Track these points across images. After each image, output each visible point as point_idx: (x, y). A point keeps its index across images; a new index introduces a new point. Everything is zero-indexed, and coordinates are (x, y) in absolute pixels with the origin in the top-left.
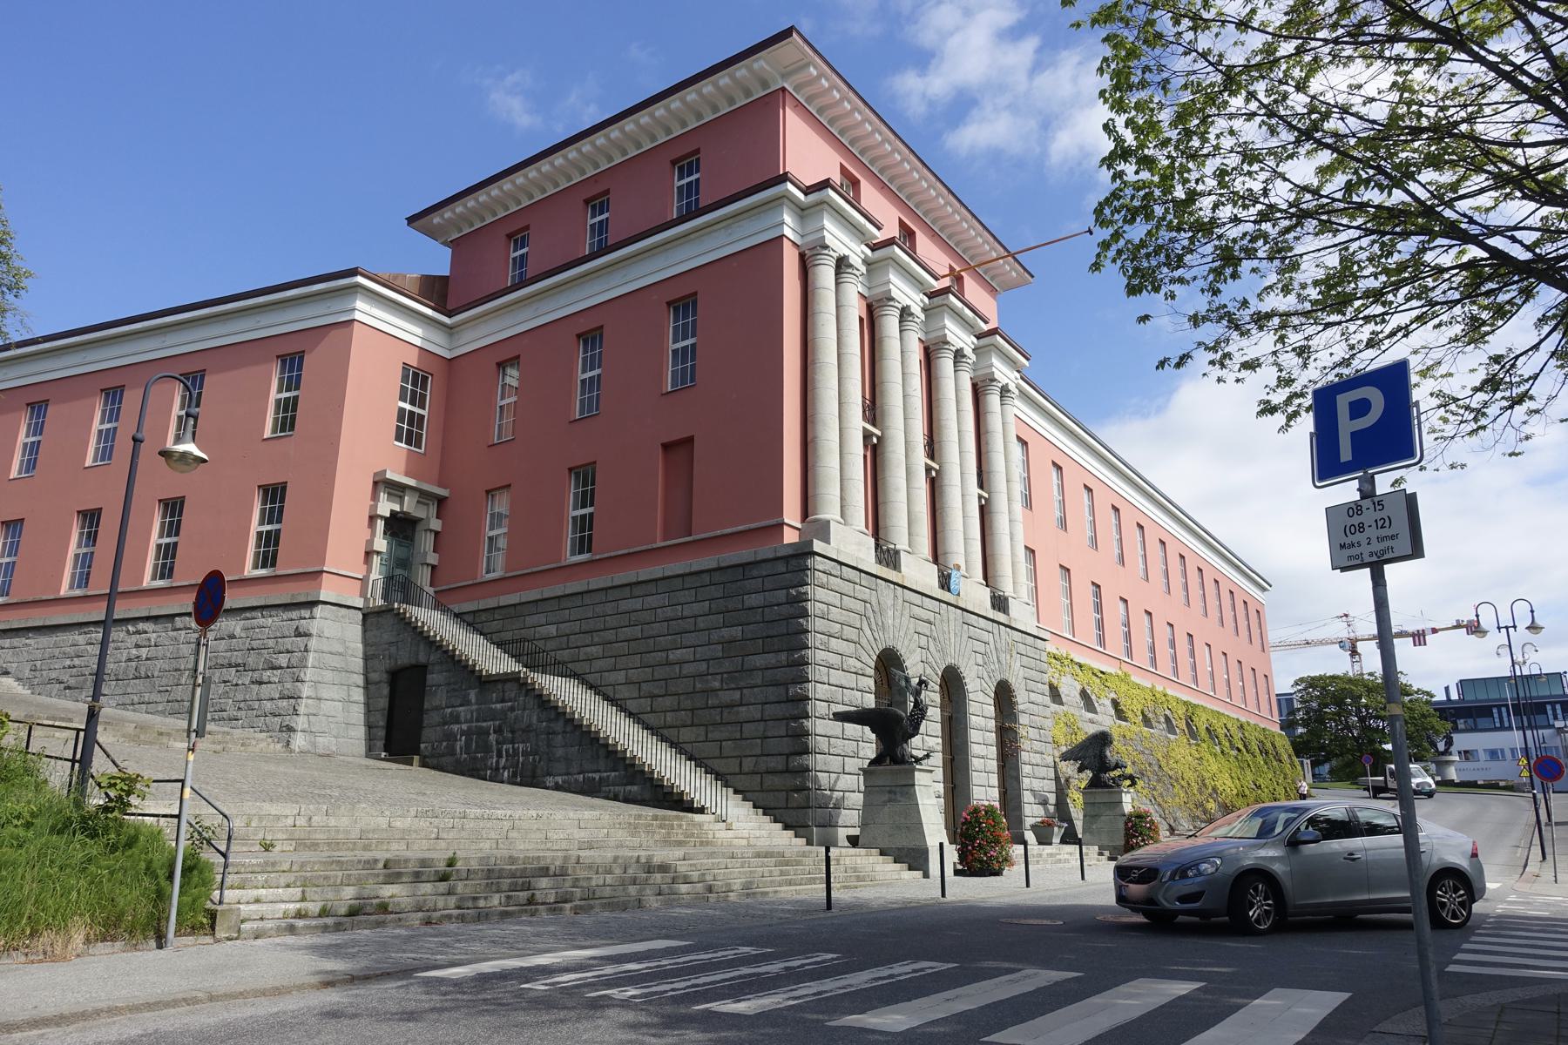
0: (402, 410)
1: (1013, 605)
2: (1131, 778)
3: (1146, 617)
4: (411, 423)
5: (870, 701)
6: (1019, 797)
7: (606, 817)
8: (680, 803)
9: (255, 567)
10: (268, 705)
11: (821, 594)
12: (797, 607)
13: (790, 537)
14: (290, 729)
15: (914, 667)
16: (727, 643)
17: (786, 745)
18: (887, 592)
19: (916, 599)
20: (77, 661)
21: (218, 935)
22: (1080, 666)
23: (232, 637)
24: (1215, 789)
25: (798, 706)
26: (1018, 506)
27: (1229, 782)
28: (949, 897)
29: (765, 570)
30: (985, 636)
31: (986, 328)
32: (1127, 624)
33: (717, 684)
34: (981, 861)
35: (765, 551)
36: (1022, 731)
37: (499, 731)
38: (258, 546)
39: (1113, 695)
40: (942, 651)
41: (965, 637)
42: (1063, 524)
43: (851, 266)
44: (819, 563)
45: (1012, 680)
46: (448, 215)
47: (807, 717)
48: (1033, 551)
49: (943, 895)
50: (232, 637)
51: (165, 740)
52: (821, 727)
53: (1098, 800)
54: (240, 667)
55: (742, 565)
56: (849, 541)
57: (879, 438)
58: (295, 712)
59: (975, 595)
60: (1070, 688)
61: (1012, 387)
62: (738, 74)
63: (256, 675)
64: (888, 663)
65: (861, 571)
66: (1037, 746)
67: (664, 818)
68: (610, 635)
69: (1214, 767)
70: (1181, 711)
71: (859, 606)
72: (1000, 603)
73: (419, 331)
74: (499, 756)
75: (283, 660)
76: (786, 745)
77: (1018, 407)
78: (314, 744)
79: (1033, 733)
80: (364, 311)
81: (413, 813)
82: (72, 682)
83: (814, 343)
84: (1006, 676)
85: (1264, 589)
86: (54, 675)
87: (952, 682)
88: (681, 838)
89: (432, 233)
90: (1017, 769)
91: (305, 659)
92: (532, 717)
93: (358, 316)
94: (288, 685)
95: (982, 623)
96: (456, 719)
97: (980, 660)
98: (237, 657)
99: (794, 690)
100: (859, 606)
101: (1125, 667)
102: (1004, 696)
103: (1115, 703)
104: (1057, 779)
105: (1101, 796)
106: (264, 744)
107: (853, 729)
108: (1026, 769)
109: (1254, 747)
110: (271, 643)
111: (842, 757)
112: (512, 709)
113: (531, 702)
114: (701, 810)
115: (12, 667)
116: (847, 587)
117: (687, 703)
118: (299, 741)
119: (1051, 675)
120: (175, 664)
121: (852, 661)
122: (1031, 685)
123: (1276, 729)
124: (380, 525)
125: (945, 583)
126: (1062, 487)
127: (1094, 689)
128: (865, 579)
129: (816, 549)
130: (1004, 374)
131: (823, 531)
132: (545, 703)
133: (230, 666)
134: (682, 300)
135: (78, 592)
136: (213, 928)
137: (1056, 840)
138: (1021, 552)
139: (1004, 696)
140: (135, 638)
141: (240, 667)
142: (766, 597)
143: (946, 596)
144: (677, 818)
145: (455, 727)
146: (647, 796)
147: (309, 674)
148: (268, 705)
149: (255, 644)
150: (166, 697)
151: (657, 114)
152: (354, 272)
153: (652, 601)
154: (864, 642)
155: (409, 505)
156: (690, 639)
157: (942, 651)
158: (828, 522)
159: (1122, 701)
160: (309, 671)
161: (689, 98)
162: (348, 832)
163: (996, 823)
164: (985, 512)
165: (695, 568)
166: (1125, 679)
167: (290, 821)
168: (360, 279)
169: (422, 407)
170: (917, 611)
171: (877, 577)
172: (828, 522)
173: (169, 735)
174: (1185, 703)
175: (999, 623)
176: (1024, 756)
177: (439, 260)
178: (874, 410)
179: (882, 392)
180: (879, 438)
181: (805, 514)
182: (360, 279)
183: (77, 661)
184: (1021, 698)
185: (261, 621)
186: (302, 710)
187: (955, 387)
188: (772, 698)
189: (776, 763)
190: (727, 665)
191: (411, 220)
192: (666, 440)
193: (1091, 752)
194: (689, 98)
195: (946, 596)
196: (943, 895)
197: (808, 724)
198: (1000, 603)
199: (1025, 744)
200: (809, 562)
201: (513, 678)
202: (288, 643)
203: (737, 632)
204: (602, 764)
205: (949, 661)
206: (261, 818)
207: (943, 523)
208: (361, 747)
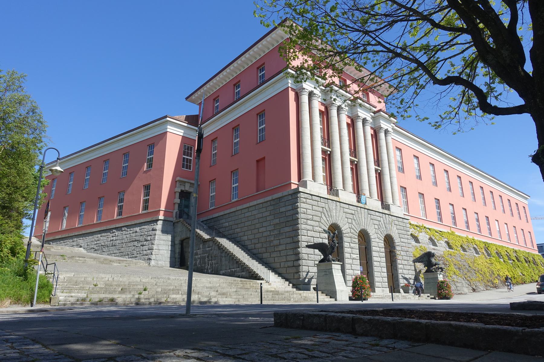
0: (184, 158)
1: (392, 208)
2: (441, 268)
3: (464, 211)
4: (187, 162)
5: (326, 241)
6: (397, 276)
7: (222, 281)
8: (254, 276)
10: (145, 252)
11: (303, 205)
12: (295, 210)
13: (293, 187)
14: (150, 259)
15: (345, 228)
17: (293, 258)
18: (332, 205)
19: (347, 206)
20: (98, 242)
22: (429, 229)
23: (136, 232)
24: (498, 275)
26: (394, 172)
28: (320, 303)
30: (379, 219)
32: (454, 213)
33: (272, 239)
34: (358, 295)
36: (398, 253)
37: (208, 257)
39: (446, 240)
41: (369, 219)
43: (315, 94)
44: (302, 195)
45: (393, 235)
47: (299, 248)
51: (111, 263)
52: (304, 251)
54: (138, 241)
55: (279, 198)
56: (316, 187)
57: (330, 152)
58: (152, 254)
60: (423, 237)
61: (390, 129)
63: (142, 243)
64: (335, 231)
65: (321, 197)
67: (245, 281)
69: (499, 267)
71: (321, 209)
72: (385, 206)
73: (183, 131)
75: (149, 238)
76: (293, 258)
77: (393, 135)
78: (158, 264)
79: (402, 253)
81: (150, 278)
82: (97, 248)
83: (301, 122)
84: (389, 233)
85: (526, 199)
86: (92, 246)
87: (364, 237)
89: (193, 102)
90: (396, 266)
91: (155, 237)
92: (216, 252)
93: (168, 130)
96: (196, 254)
97: (376, 227)
98: (137, 238)
99: (295, 240)
100: (321, 209)
101: (453, 230)
102: (389, 241)
103: (448, 243)
104: (415, 270)
105: (430, 275)
106: (142, 263)
107: (311, 251)
108: (400, 266)
109: (522, 259)
110: (146, 233)
111: (310, 261)
112: (211, 250)
113: (216, 248)
114: (262, 279)
115: (82, 245)
117: (265, 245)
118: (153, 263)
122: (401, 236)
123: (537, 253)
124: (177, 195)
125: (359, 201)
128: (322, 200)
129: (300, 190)
130: (384, 125)
131: (305, 185)
132: (221, 248)
133: (135, 241)
134: (260, 113)
135: (99, 222)
137: (411, 291)
138: (397, 189)
139: (389, 241)
141: (138, 241)
142: (285, 207)
143: (360, 205)
144: (245, 281)
145: (197, 257)
146: (247, 275)
147: (156, 242)
149: (142, 234)
150: (119, 251)
151: (255, 50)
152: (166, 117)
154: (322, 221)
155: (187, 188)
157: (359, 224)
158: (306, 181)
159: (451, 242)
160: (156, 241)
161: (264, 43)
162: (124, 282)
163: (363, 282)
164: (380, 176)
165: (266, 200)
166: (453, 234)
167: (107, 279)
169: (191, 156)
170: (346, 210)
171: (328, 199)
173: (113, 261)
174: (484, 243)
176: (399, 262)
177: (194, 110)
178: (354, 152)
180: (330, 152)
181: (300, 178)
182: (168, 119)
183: (98, 242)
184: (397, 240)
185: (144, 227)
186: (153, 253)
189: (290, 264)
191: (187, 98)
194: (264, 43)
195: (360, 205)
197: (299, 250)
198: (385, 206)
199: (399, 257)
202: (151, 233)
203: (277, 221)
204: (235, 266)
205: (362, 227)
207: (361, 180)
208: (168, 264)
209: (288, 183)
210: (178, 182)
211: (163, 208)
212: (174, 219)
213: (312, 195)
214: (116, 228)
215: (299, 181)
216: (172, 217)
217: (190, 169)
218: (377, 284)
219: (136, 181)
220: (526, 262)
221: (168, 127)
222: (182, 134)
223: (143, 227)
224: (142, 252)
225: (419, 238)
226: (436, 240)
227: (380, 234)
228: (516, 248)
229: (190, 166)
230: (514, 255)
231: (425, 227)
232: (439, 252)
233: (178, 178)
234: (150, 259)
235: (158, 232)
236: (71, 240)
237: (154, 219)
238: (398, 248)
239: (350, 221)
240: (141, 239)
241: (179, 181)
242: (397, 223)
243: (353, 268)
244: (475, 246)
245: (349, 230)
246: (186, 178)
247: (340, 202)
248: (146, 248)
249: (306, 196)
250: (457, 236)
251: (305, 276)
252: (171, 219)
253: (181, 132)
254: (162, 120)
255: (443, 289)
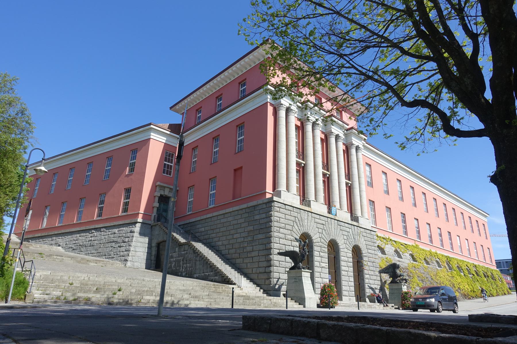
0: (165, 164)
3: (428, 226)
4: (168, 168)
6: (364, 286)
7: (195, 284)
8: (227, 281)
9: (122, 212)
10: (122, 253)
11: (276, 214)
12: (269, 218)
13: (268, 196)
14: (126, 260)
15: (315, 238)
16: (249, 232)
18: (304, 215)
19: (318, 217)
20: (76, 242)
21: (26, 301)
22: (395, 242)
23: (115, 233)
24: (459, 288)
25: (268, 250)
26: (364, 186)
27: (467, 286)
28: (289, 309)
29: (260, 207)
30: (348, 230)
31: (348, 127)
32: (418, 228)
33: (246, 245)
34: (326, 303)
35: (260, 202)
36: (365, 263)
37: (183, 260)
38: (124, 206)
39: (411, 252)
40: (329, 234)
41: (339, 230)
42: (387, 192)
44: (276, 204)
46: (183, 104)
48: (374, 202)
49: (287, 308)
50: (115, 233)
52: (276, 258)
53: (394, 288)
54: (116, 242)
55: (254, 206)
56: (290, 197)
58: (128, 255)
59: (344, 215)
61: (361, 146)
62: (255, 55)
63: (120, 244)
66: (372, 268)
68: (218, 230)
69: (459, 280)
70: (445, 259)
71: (293, 218)
73: (165, 139)
74: (183, 268)
75: (127, 240)
76: (265, 264)
80: (153, 136)
82: (75, 248)
84: (357, 243)
86: (71, 246)
87: (333, 247)
88: (221, 291)
89: (177, 111)
90: (363, 276)
91: (132, 239)
93: (152, 137)
94: (127, 247)
95: (347, 225)
97: (345, 237)
98: (115, 239)
100: (293, 218)
102: (357, 251)
103: (412, 256)
104: (381, 280)
105: (395, 286)
106: (118, 264)
107: (282, 258)
108: (366, 276)
109: (481, 273)
110: (124, 235)
111: (281, 268)
113: (192, 252)
114: (234, 284)
115: (61, 244)
116: (288, 212)
118: (129, 264)
119: (378, 243)
120: (100, 242)
121: (289, 237)
122: (369, 247)
123: (495, 268)
124: (157, 199)
125: (330, 212)
126: (387, 180)
127: (401, 250)
130: (356, 142)
131: (279, 195)
132: (196, 252)
133: (113, 242)
134: (240, 125)
136: (25, 299)
138: (365, 202)
139: (357, 251)
140: (91, 235)
141: (116, 242)
142: (260, 214)
143: (330, 216)
144: (217, 285)
145: (172, 260)
146: (220, 280)
147: (133, 244)
148: (122, 253)
149: (120, 235)
152: (150, 124)
153: (230, 219)
154: (294, 230)
155: (167, 193)
156: (239, 231)
157: (329, 234)
158: (280, 191)
159: (415, 254)
160: (133, 243)
162: (100, 282)
164: (350, 189)
166: (417, 247)
168: (152, 126)
169: (172, 163)
170: (317, 220)
171: (300, 209)
172: (280, 191)
175: (354, 225)
177: (178, 119)
178: (327, 165)
179: (306, 149)
182: (152, 126)
183: (76, 242)
184: (364, 251)
186: (130, 254)
187: (337, 150)
188: (261, 249)
189: (262, 270)
190: (250, 239)
191: (171, 108)
192: (235, 168)
193: (390, 270)
195: (330, 216)
196: (287, 308)
197: (271, 256)
199: (366, 267)
200: (273, 204)
201: (416, 310)
203: (251, 228)
205: (332, 237)
206: (73, 277)
209: (263, 192)
210: (158, 187)
211: (142, 211)
212: (152, 222)
213: (285, 205)
214: (95, 229)
215: (273, 191)
216: (150, 220)
217: (170, 174)
218: (344, 293)
219: (117, 184)
220: (485, 276)
221: (152, 134)
222: (164, 141)
223: (121, 229)
224: (119, 253)
225: (385, 250)
226: (401, 253)
227: (349, 244)
228: (476, 263)
229: (170, 172)
230: (474, 269)
231: (391, 240)
232: (404, 264)
233: (158, 183)
234: (126, 260)
235: (136, 235)
236: (50, 239)
237: (133, 221)
238: (365, 259)
239: (320, 231)
240: (119, 240)
241: (159, 185)
242: (364, 234)
243: (322, 277)
244: (438, 259)
245: (319, 240)
246: (164, 183)
247: (312, 213)
248: (123, 249)
249: (280, 205)
250: (421, 249)
251: (275, 282)
252: (149, 222)
253: (163, 139)
254: (146, 127)
255: (406, 299)
